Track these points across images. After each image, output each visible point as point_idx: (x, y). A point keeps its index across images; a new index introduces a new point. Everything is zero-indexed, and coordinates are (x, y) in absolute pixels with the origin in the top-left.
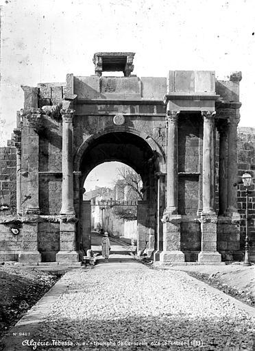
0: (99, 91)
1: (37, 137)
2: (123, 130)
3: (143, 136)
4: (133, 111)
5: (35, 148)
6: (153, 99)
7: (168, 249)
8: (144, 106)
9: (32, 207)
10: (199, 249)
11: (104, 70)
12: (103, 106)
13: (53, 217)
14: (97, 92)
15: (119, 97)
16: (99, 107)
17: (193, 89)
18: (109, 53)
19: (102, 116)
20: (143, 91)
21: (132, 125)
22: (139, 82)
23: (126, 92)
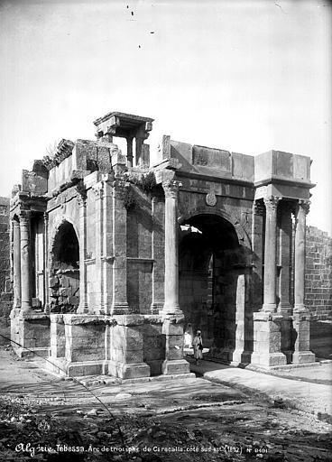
0: (191, 162)
1: (125, 212)
2: (213, 212)
3: (233, 220)
4: (224, 190)
5: (123, 226)
6: (243, 179)
7: (101, 366)
8: (234, 187)
9: (120, 303)
10: (163, 358)
11: (116, 135)
12: (195, 181)
13: (155, 316)
14: (188, 163)
15: (212, 173)
16: (191, 181)
17: (291, 174)
18: (128, 115)
19: (194, 192)
20: (235, 168)
21: (223, 207)
22: (230, 158)
23: (216, 167)
